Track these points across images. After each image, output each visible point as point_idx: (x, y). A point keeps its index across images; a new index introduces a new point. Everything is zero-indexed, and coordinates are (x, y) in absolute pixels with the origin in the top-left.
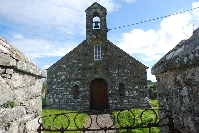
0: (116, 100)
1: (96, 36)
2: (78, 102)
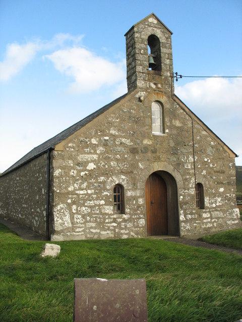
0: (191, 214)
2: (125, 221)
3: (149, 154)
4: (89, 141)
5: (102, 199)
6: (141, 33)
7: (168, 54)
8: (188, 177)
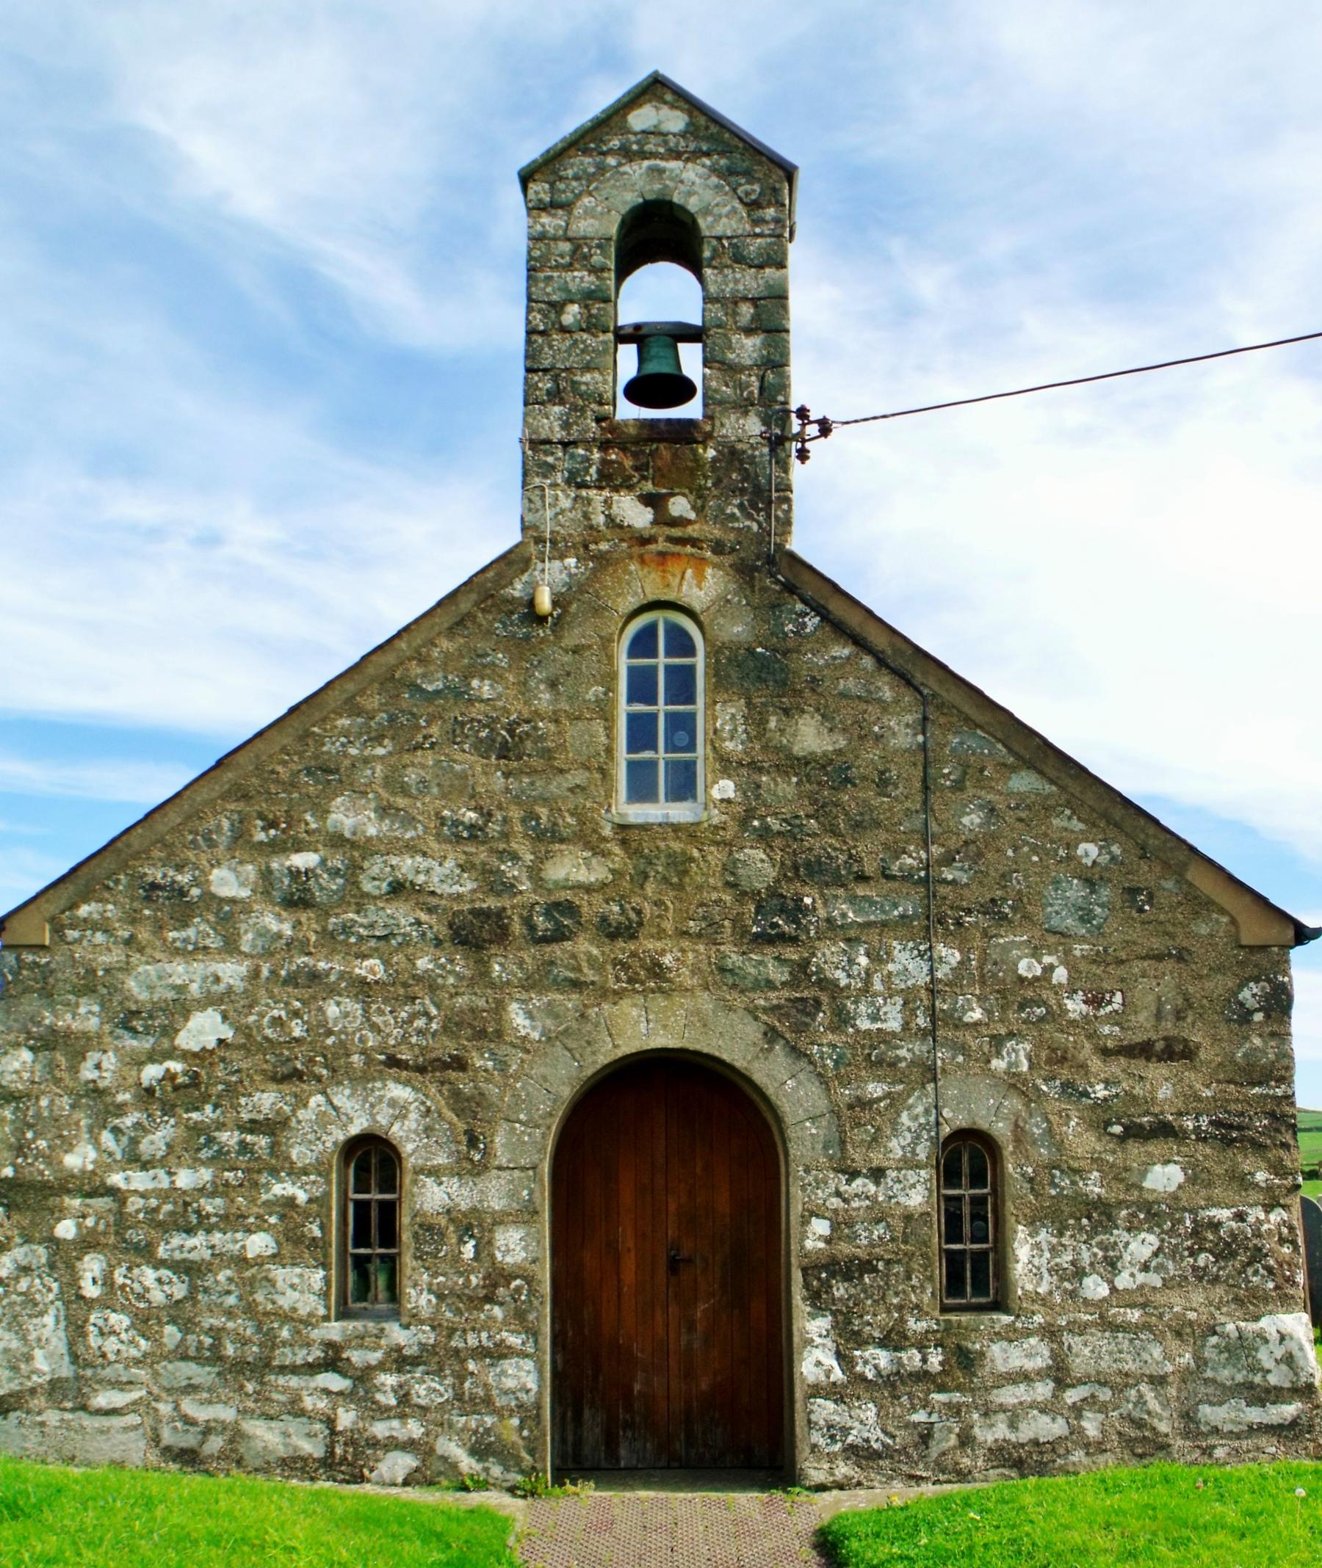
0: (893, 1339)
1: (648, 500)
2: (400, 1361)
3: (585, 946)
4: (196, 882)
5: (261, 1226)
6: (567, 206)
7: (754, 301)
8: (875, 1089)
